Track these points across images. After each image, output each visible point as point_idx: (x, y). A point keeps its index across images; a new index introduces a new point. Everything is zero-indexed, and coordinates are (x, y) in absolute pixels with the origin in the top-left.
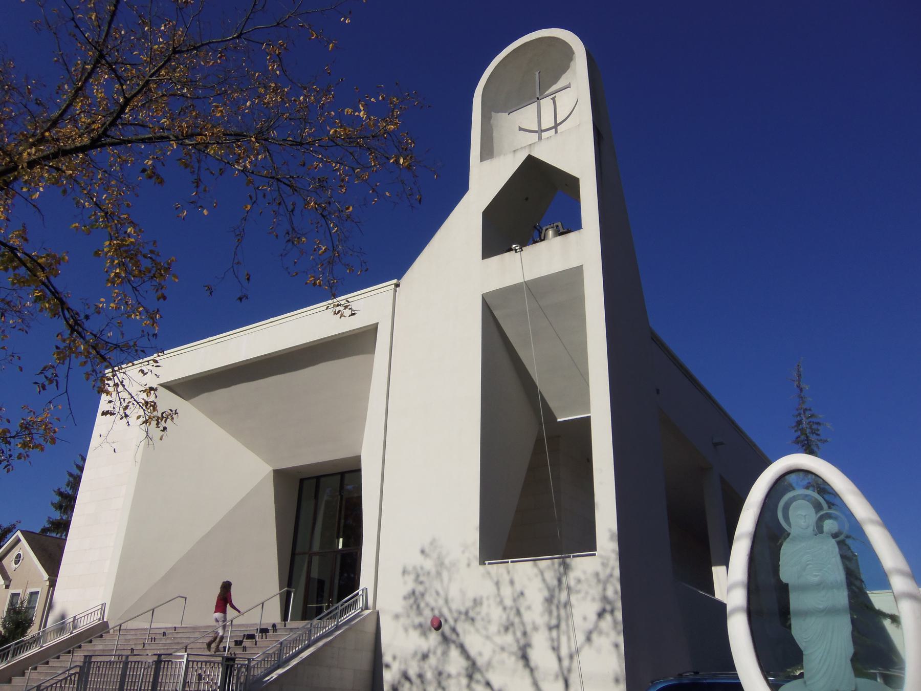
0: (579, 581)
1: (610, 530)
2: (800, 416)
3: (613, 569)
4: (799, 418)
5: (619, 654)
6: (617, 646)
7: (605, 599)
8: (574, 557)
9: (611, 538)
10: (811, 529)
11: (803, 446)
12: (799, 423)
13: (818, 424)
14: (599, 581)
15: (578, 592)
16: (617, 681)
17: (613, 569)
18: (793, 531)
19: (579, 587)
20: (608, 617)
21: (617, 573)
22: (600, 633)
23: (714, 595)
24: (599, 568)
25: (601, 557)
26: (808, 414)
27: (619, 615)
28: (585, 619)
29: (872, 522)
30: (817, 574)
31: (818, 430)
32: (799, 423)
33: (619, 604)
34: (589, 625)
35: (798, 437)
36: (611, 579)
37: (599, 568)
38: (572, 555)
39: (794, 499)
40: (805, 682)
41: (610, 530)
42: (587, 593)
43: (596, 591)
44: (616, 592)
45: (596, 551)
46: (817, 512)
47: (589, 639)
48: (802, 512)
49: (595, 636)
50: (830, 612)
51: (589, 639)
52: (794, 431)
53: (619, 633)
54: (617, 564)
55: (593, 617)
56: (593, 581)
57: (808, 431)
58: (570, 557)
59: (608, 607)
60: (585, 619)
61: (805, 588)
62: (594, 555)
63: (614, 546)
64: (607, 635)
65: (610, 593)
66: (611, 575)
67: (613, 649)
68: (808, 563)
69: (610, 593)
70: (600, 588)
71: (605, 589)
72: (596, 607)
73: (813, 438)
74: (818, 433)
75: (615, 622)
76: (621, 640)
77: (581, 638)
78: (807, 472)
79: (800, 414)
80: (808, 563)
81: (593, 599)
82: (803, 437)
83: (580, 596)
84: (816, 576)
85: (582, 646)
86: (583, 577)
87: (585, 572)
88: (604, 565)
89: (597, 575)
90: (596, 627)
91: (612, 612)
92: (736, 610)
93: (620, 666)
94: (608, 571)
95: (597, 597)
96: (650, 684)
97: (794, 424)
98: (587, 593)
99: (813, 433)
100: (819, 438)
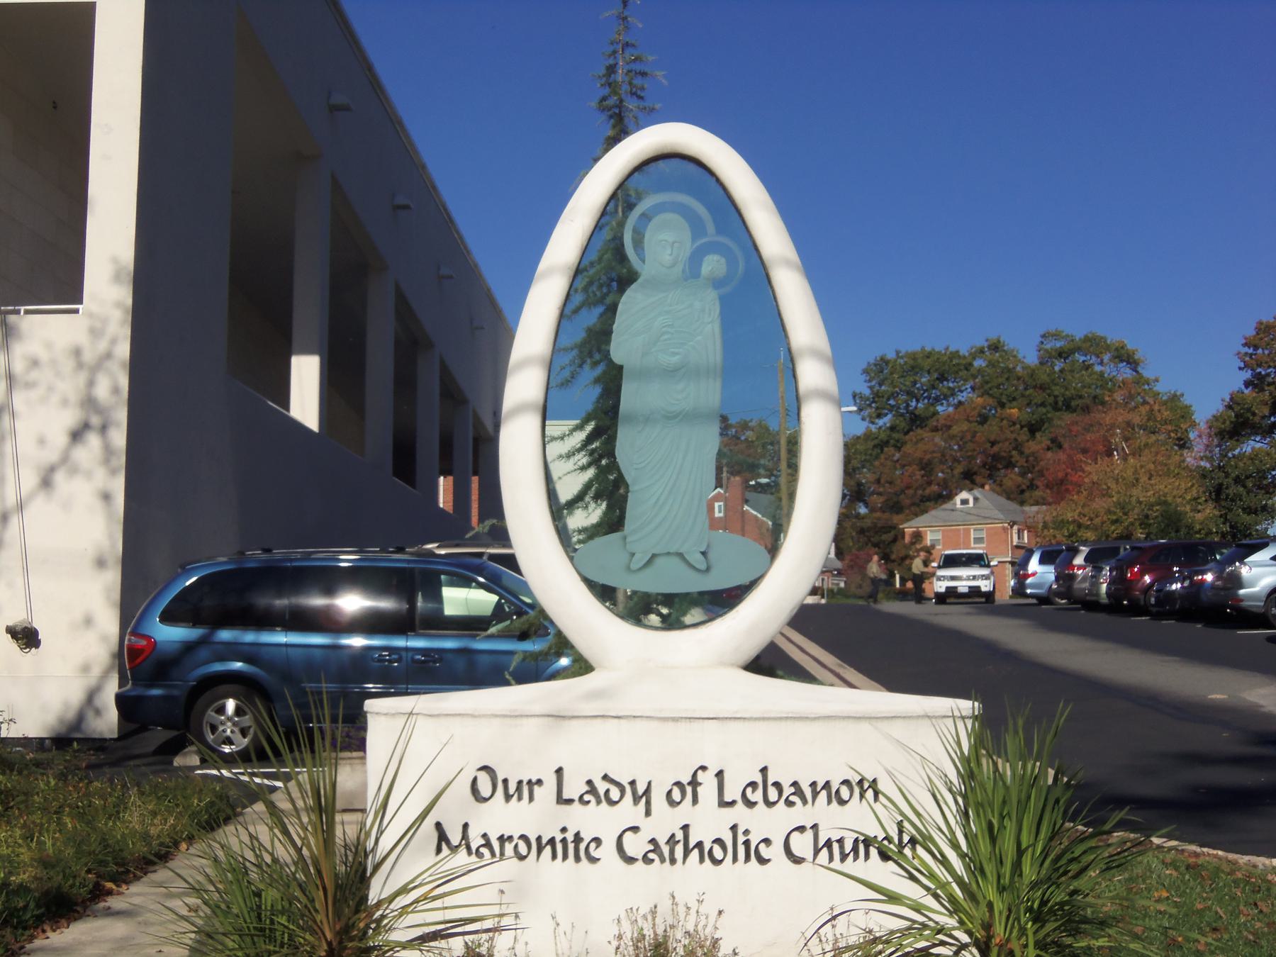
0: (35, 363)
1: (115, 260)
2: (615, 58)
3: (114, 341)
4: (611, 61)
5: (110, 516)
6: (106, 497)
7: (89, 403)
8: (27, 312)
9: (117, 278)
10: (678, 269)
11: (611, 117)
12: (611, 69)
13: (643, 74)
14: (80, 365)
15: (29, 385)
16: (101, 563)
17: (114, 341)
18: (647, 270)
19: (34, 375)
20: (93, 440)
21: (123, 350)
22: (74, 471)
23: (287, 408)
24: (82, 339)
25: (90, 315)
26: (630, 54)
27: (119, 438)
28: (42, 441)
29: (788, 263)
30: (676, 350)
31: (642, 89)
32: (611, 69)
33: (122, 415)
34: (52, 456)
35: (604, 99)
36: (109, 364)
37: (82, 339)
38: (23, 309)
39: (646, 217)
40: (625, 538)
41: (115, 260)
42: (51, 389)
43: (71, 386)
44: (116, 390)
45: (81, 303)
46: (694, 239)
47: (46, 482)
48: (667, 236)
49: (60, 477)
50: (689, 417)
51: (46, 482)
52: (599, 85)
53: (113, 472)
54: (127, 332)
55: (59, 439)
56: (68, 365)
57: (626, 88)
58: (18, 312)
59: (95, 420)
60: (42, 441)
61: (645, 374)
62: (77, 311)
63: (124, 295)
64: (89, 475)
65: (102, 391)
66: (108, 356)
67: (98, 505)
68: (664, 329)
69: (102, 391)
70: (82, 378)
71: (91, 383)
72: (70, 418)
73: (631, 104)
74: (642, 95)
75: (108, 451)
76: (118, 486)
77: (30, 480)
78: (641, 167)
79: (615, 52)
80: (664, 329)
81: (65, 402)
82: (613, 101)
83: (34, 394)
84: (675, 354)
85: (31, 496)
86: (43, 355)
87: (49, 346)
88: (95, 333)
89: (77, 352)
90: (65, 459)
91: (104, 429)
92: (520, 409)
93: (111, 536)
94: (102, 346)
95: (74, 397)
96: (179, 570)
97: (603, 71)
98: (51, 389)
99: (633, 94)
100: (642, 104)
